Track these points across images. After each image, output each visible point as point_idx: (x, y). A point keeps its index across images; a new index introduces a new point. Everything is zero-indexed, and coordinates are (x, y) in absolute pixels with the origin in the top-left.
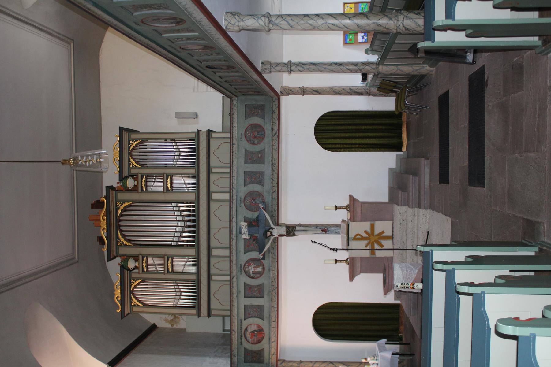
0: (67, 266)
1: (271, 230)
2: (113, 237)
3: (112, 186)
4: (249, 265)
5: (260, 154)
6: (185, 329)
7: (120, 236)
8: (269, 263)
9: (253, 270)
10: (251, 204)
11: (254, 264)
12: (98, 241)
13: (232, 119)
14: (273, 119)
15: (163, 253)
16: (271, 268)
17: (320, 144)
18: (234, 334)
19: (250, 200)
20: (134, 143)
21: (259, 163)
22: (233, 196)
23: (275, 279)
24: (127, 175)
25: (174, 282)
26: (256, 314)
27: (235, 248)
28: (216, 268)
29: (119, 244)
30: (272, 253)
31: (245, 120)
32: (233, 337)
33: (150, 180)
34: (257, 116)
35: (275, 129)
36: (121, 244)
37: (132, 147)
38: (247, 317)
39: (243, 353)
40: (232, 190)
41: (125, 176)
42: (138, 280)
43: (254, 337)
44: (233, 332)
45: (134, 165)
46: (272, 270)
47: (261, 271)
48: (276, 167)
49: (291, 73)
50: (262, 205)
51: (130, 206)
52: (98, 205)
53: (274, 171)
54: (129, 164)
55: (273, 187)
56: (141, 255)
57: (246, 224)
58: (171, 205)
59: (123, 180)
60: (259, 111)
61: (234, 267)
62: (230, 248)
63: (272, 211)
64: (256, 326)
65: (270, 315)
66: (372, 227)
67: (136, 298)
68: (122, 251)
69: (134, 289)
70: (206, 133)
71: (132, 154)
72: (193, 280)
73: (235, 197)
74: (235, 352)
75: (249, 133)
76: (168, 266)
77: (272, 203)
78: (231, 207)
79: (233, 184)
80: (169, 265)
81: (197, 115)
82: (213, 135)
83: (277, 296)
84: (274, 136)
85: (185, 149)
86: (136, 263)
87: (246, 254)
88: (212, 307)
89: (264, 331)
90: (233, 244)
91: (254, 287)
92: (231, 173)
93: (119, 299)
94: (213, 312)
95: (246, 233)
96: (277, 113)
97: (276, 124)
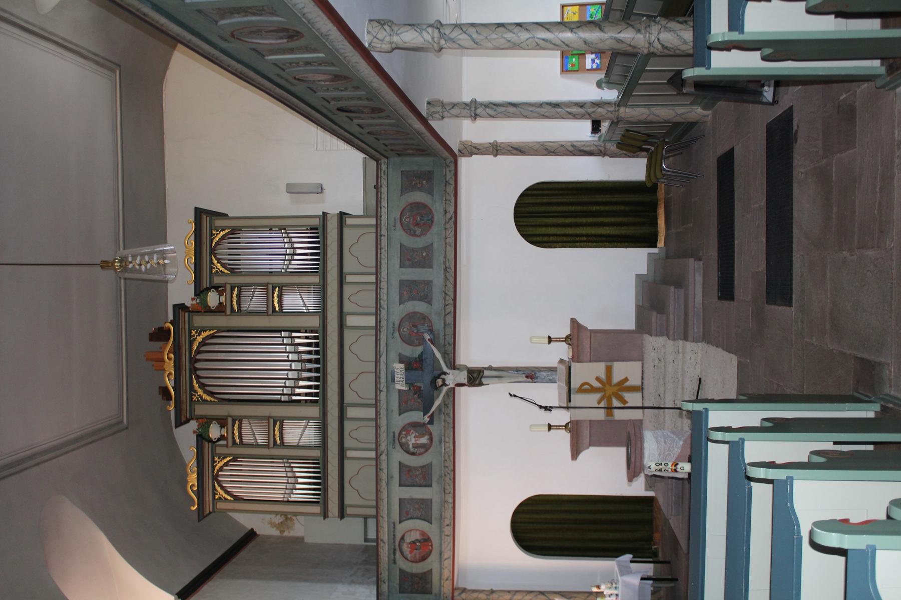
0: (110, 435)
1: (443, 376)
2: (184, 388)
3: (184, 304)
4: (408, 434)
5: (426, 252)
6: (302, 539)
7: (196, 386)
8: (441, 430)
9: (413, 441)
10: (410, 334)
11: (416, 432)
12: (160, 394)
13: (379, 194)
14: (447, 195)
15: (267, 414)
16: (443, 438)
17: (523, 235)
18: (383, 547)
19: (409, 328)
20: (219, 233)
21: (424, 267)
22: (381, 320)
23: (449, 456)
24: (208, 286)
25: (285, 460)
26: (418, 514)
27: (384, 406)
28: (354, 438)
29: (195, 398)
30: (445, 414)
31: (401, 196)
32: (382, 550)
33: (246, 294)
34: (420, 189)
35: (450, 212)
36: (197, 398)
37: (216, 240)
38: (404, 518)
39: (398, 578)
40: (380, 311)
41: (205, 287)
42: (226, 457)
43: (415, 551)
44: (382, 542)
45: (219, 270)
46: (445, 442)
47: (426, 442)
48: (451, 273)
49: (475, 119)
50: (429, 335)
51: (212, 336)
52: (160, 335)
53: (448, 279)
54: (212, 268)
55: (446, 305)
56: (230, 416)
57: (402, 366)
58: (280, 336)
59: (202, 295)
60: (424, 182)
61: (383, 436)
62: (376, 406)
63: (444, 346)
64: (418, 533)
65: (441, 516)
66: (609, 370)
67: (223, 488)
68: (200, 410)
69: (220, 473)
70: (336, 217)
71: (216, 252)
72: (315, 458)
73: (384, 323)
74: (384, 575)
75: (407, 218)
76: (274, 435)
77: (445, 333)
78: (378, 338)
79: (382, 301)
80: (277, 433)
81: (322, 189)
82: (349, 221)
83: (452, 484)
84: (449, 222)
85: (302, 244)
86: (223, 429)
87: (402, 416)
88: (347, 501)
89: (431, 542)
90: (381, 399)
91: (416, 468)
92: (377, 283)
93: (195, 489)
94: (349, 511)
95: (402, 381)
96: (454, 185)
97: (451, 202)
